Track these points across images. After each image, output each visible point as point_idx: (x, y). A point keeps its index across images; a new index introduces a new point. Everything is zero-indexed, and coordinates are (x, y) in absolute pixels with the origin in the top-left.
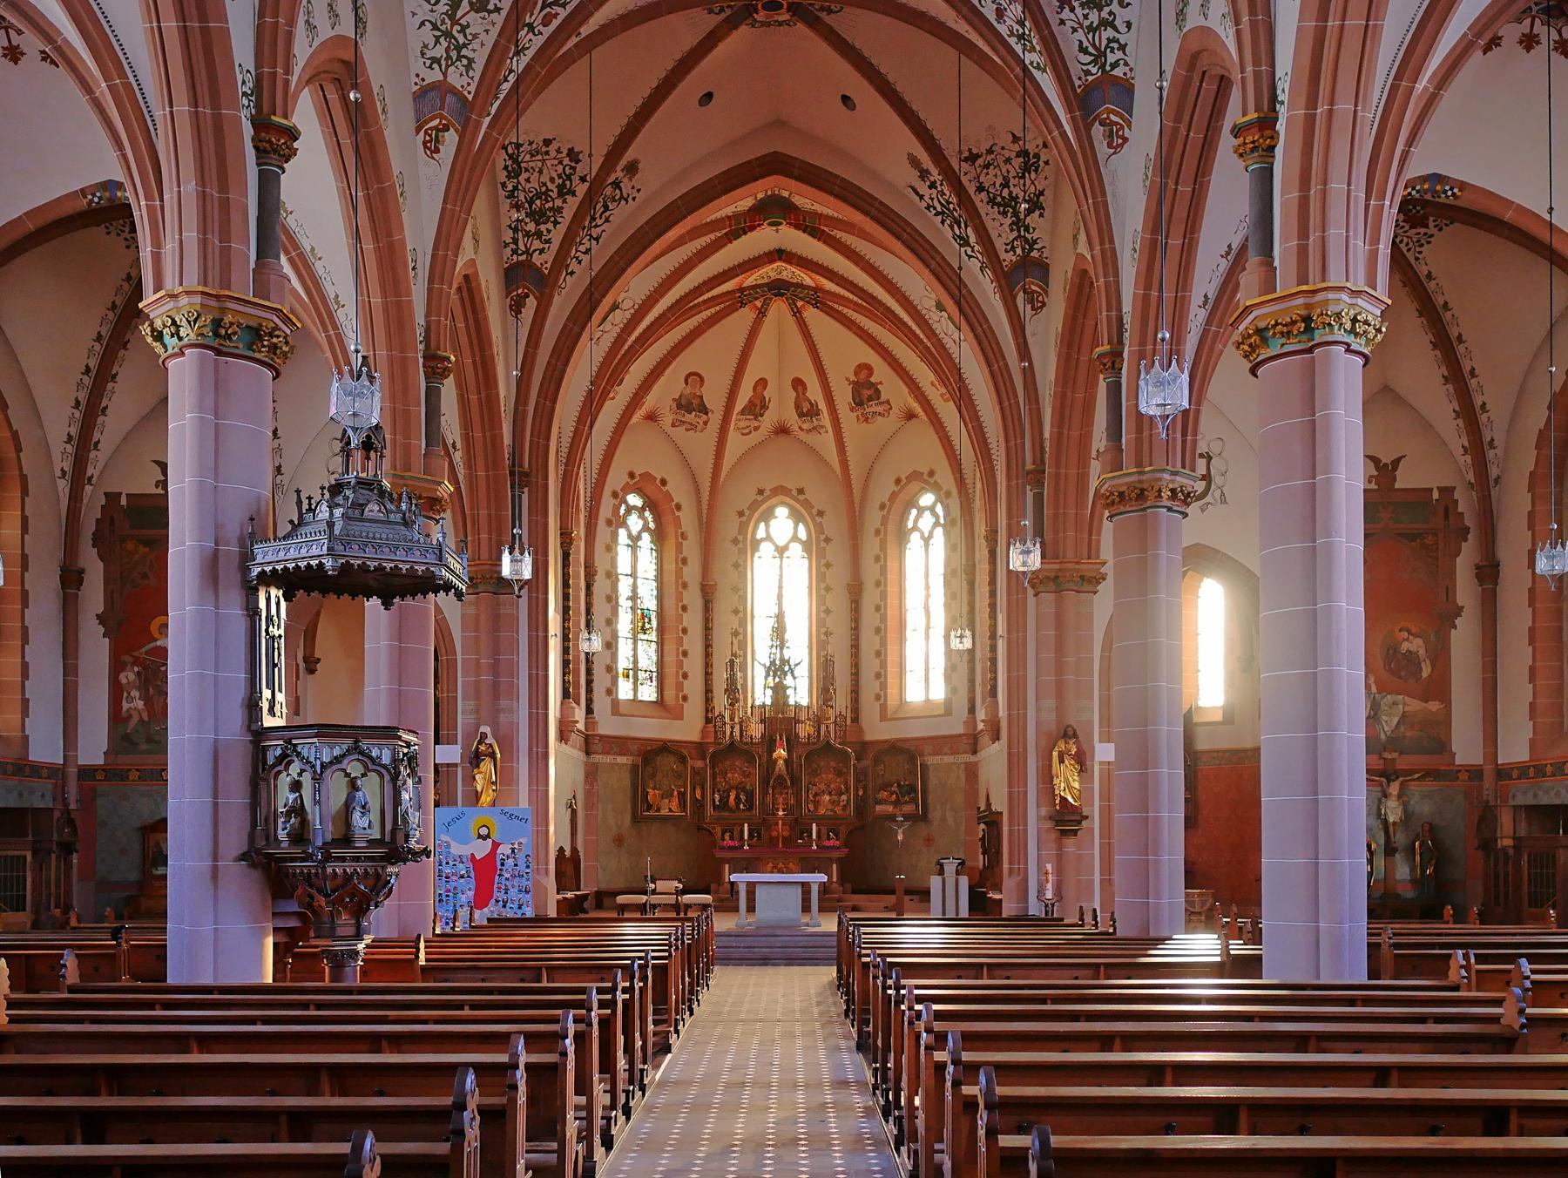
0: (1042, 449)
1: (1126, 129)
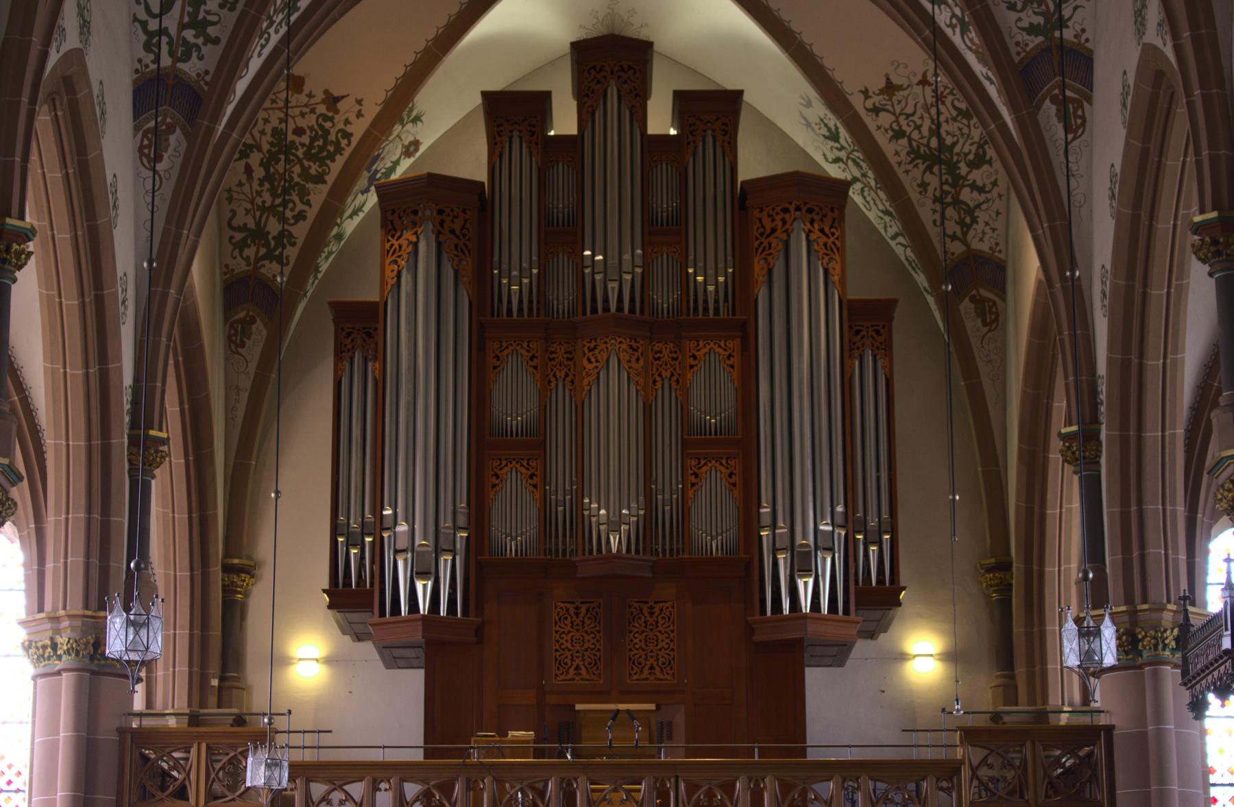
0: (1094, 392)
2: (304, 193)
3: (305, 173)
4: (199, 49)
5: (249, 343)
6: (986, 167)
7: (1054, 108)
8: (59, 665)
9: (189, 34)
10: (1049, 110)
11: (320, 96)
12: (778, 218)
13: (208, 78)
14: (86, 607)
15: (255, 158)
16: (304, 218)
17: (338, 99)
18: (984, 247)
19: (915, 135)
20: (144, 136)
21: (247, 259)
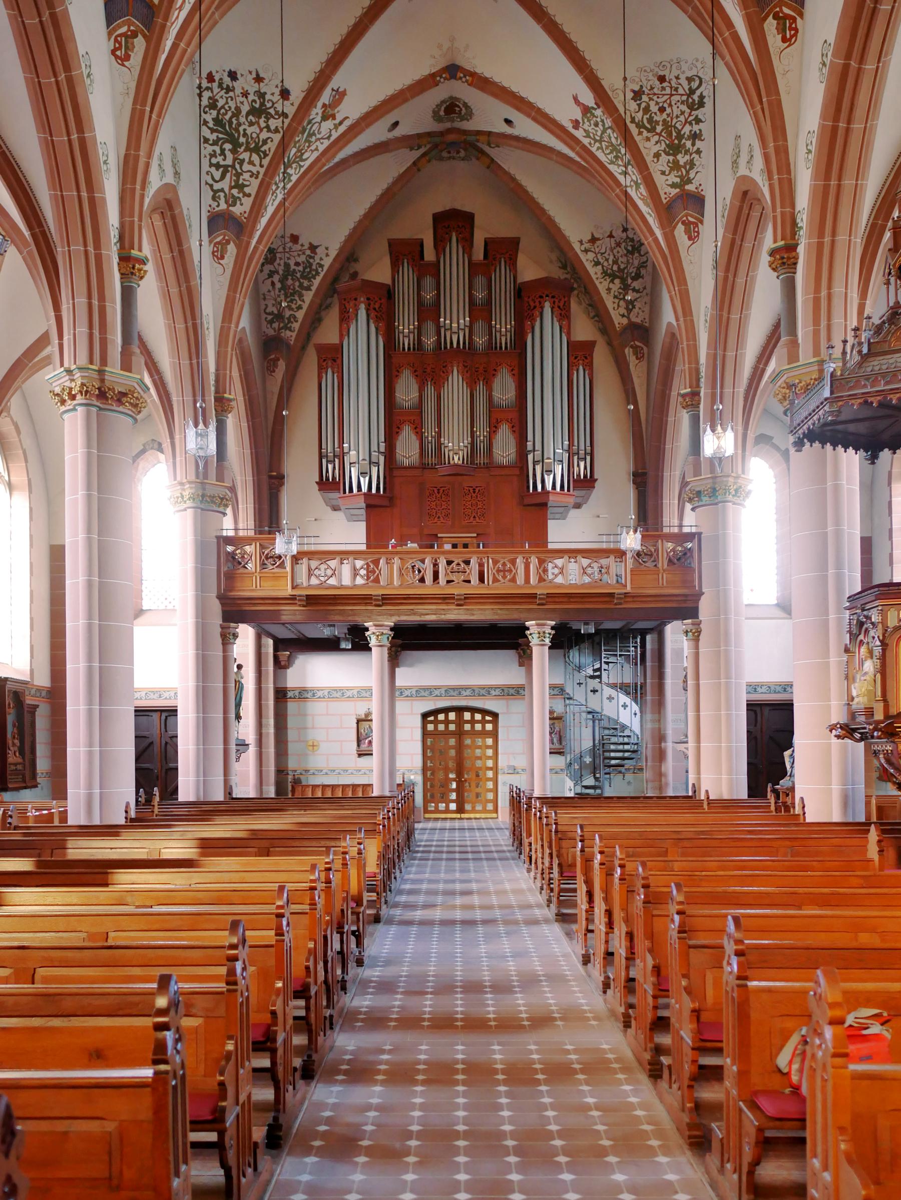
1: (799, 19)
2: (301, 296)
3: (301, 286)
4: (240, 200)
5: (277, 370)
6: (640, 280)
7: (683, 227)
8: (185, 506)
9: (235, 192)
10: (680, 230)
11: (307, 246)
12: (537, 301)
13: (246, 215)
14: (197, 477)
15: (276, 278)
16: (301, 308)
17: (317, 247)
18: (638, 320)
19: (605, 264)
20: (215, 246)
21: (274, 329)
